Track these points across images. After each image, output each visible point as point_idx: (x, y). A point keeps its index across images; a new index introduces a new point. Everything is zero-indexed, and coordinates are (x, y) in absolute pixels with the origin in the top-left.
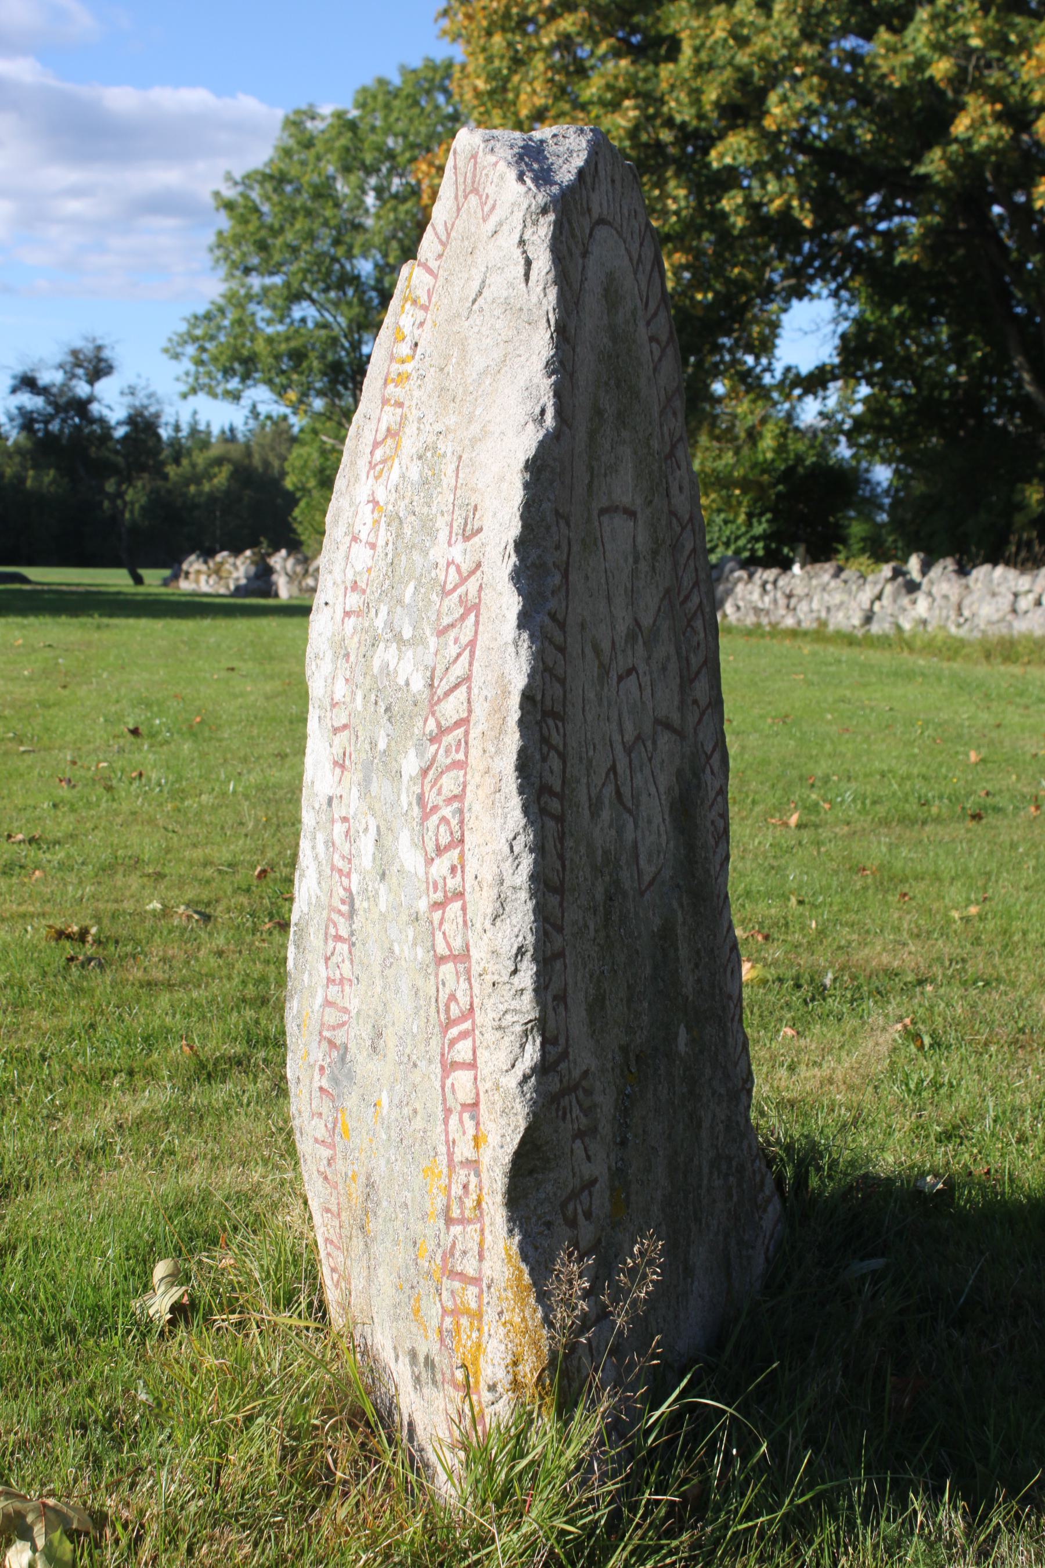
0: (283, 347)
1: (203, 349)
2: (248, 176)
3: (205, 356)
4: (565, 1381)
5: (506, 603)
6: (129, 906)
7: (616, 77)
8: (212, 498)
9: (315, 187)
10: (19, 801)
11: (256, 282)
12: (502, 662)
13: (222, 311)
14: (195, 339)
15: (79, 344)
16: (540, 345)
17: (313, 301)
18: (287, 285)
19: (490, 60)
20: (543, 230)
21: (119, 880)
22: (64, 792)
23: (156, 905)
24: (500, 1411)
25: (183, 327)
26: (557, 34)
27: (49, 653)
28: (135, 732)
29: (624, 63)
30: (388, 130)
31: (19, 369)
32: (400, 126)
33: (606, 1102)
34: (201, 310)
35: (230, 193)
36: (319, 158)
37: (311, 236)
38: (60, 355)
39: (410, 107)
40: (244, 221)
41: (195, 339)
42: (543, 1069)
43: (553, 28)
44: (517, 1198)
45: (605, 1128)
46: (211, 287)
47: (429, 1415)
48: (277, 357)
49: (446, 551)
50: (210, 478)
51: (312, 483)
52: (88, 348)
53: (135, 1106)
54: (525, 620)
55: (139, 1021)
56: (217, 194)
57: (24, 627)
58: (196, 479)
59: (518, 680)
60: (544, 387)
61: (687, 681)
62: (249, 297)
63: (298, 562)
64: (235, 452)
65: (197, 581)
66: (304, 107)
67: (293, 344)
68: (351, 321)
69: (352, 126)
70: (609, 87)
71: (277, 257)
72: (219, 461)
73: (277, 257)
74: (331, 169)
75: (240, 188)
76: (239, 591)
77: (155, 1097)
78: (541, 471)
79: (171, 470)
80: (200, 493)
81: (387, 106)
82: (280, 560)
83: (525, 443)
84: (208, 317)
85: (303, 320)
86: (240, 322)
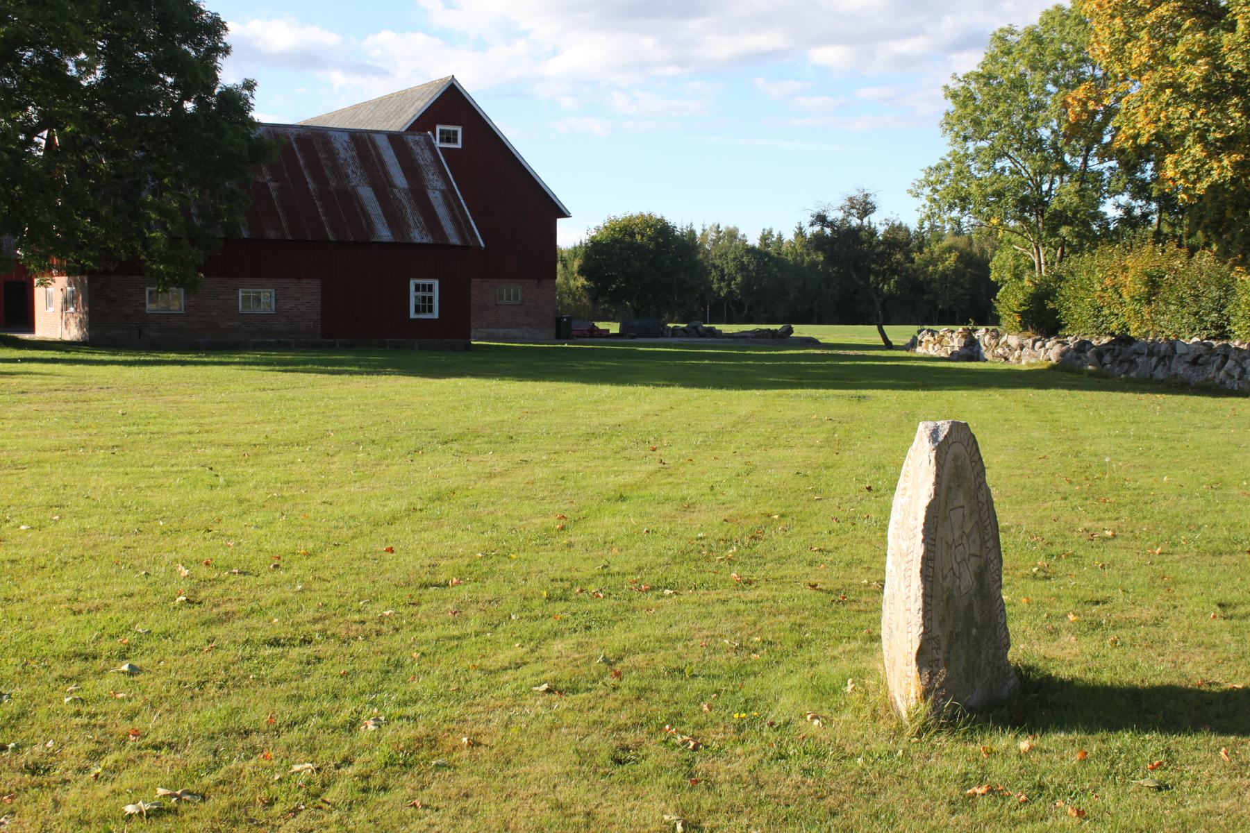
0: (989, 190)
1: (935, 191)
2: (967, 76)
3: (936, 197)
4: (925, 695)
5: (920, 537)
6: (856, 581)
7: (1193, 45)
8: (944, 275)
9: (1011, 81)
10: (815, 529)
11: (971, 146)
12: (919, 550)
13: (949, 166)
14: (930, 183)
15: (853, 193)
16: (932, 479)
17: (1010, 157)
18: (992, 147)
19: (1112, 34)
20: (933, 454)
21: (854, 569)
22: (835, 525)
23: (866, 581)
24: (913, 703)
25: (922, 176)
26: (1157, 17)
27: (829, 425)
28: (869, 489)
29: (1198, 36)
30: (1063, 40)
31: (816, 210)
32: (1069, 39)
33: (944, 643)
34: (934, 165)
35: (956, 86)
36: (1015, 62)
37: (1008, 114)
38: (843, 202)
39: (1078, 25)
40: (964, 105)
41: (930, 183)
42: (924, 633)
43: (1153, 13)
44: (917, 659)
45: (943, 648)
46: (940, 147)
47: (902, 708)
48: (985, 196)
49: (912, 521)
50: (943, 262)
51: (1008, 276)
52: (859, 196)
53: (848, 647)
54: (923, 541)
55: (856, 622)
56: (946, 87)
57: (816, 399)
58: (933, 261)
59: (921, 554)
60: (932, 488)
61: (983, 543)
62: (966, 156)
63: (992, 337)
64: (961, 242)
65: (927, 348)
66: (1006, 26)
67: (995, 186)
68: (1034, 170)
69: (1038, 40)
70: (1188, 51)
71: (986, 129)
72: (950, 249)
73: (986, 129)
74: (1022, 69)
75: (962, 84)
76: (954, 357)
77: (853, 645)
78: (930, 508)
79: (916, 256)
80: (936, 271)
81: (1062, 25)
82: (981, 333)
83: (926, 501)
84: (938, 169)
85: (1003, 169)
86: (960, 172)
